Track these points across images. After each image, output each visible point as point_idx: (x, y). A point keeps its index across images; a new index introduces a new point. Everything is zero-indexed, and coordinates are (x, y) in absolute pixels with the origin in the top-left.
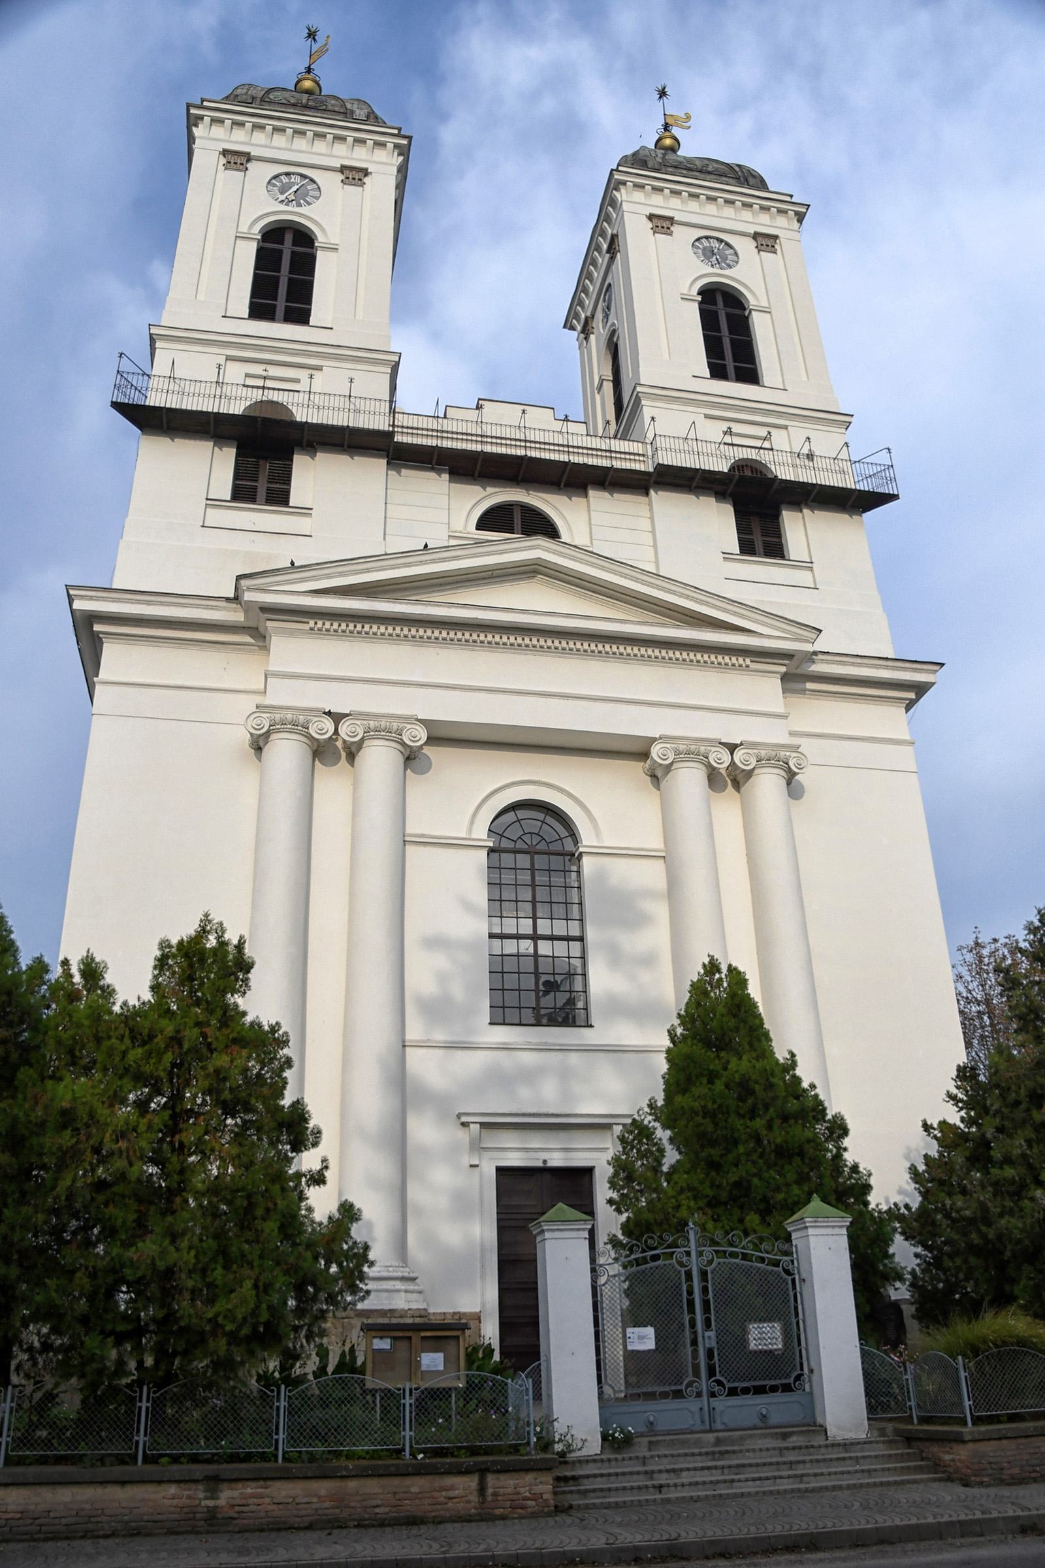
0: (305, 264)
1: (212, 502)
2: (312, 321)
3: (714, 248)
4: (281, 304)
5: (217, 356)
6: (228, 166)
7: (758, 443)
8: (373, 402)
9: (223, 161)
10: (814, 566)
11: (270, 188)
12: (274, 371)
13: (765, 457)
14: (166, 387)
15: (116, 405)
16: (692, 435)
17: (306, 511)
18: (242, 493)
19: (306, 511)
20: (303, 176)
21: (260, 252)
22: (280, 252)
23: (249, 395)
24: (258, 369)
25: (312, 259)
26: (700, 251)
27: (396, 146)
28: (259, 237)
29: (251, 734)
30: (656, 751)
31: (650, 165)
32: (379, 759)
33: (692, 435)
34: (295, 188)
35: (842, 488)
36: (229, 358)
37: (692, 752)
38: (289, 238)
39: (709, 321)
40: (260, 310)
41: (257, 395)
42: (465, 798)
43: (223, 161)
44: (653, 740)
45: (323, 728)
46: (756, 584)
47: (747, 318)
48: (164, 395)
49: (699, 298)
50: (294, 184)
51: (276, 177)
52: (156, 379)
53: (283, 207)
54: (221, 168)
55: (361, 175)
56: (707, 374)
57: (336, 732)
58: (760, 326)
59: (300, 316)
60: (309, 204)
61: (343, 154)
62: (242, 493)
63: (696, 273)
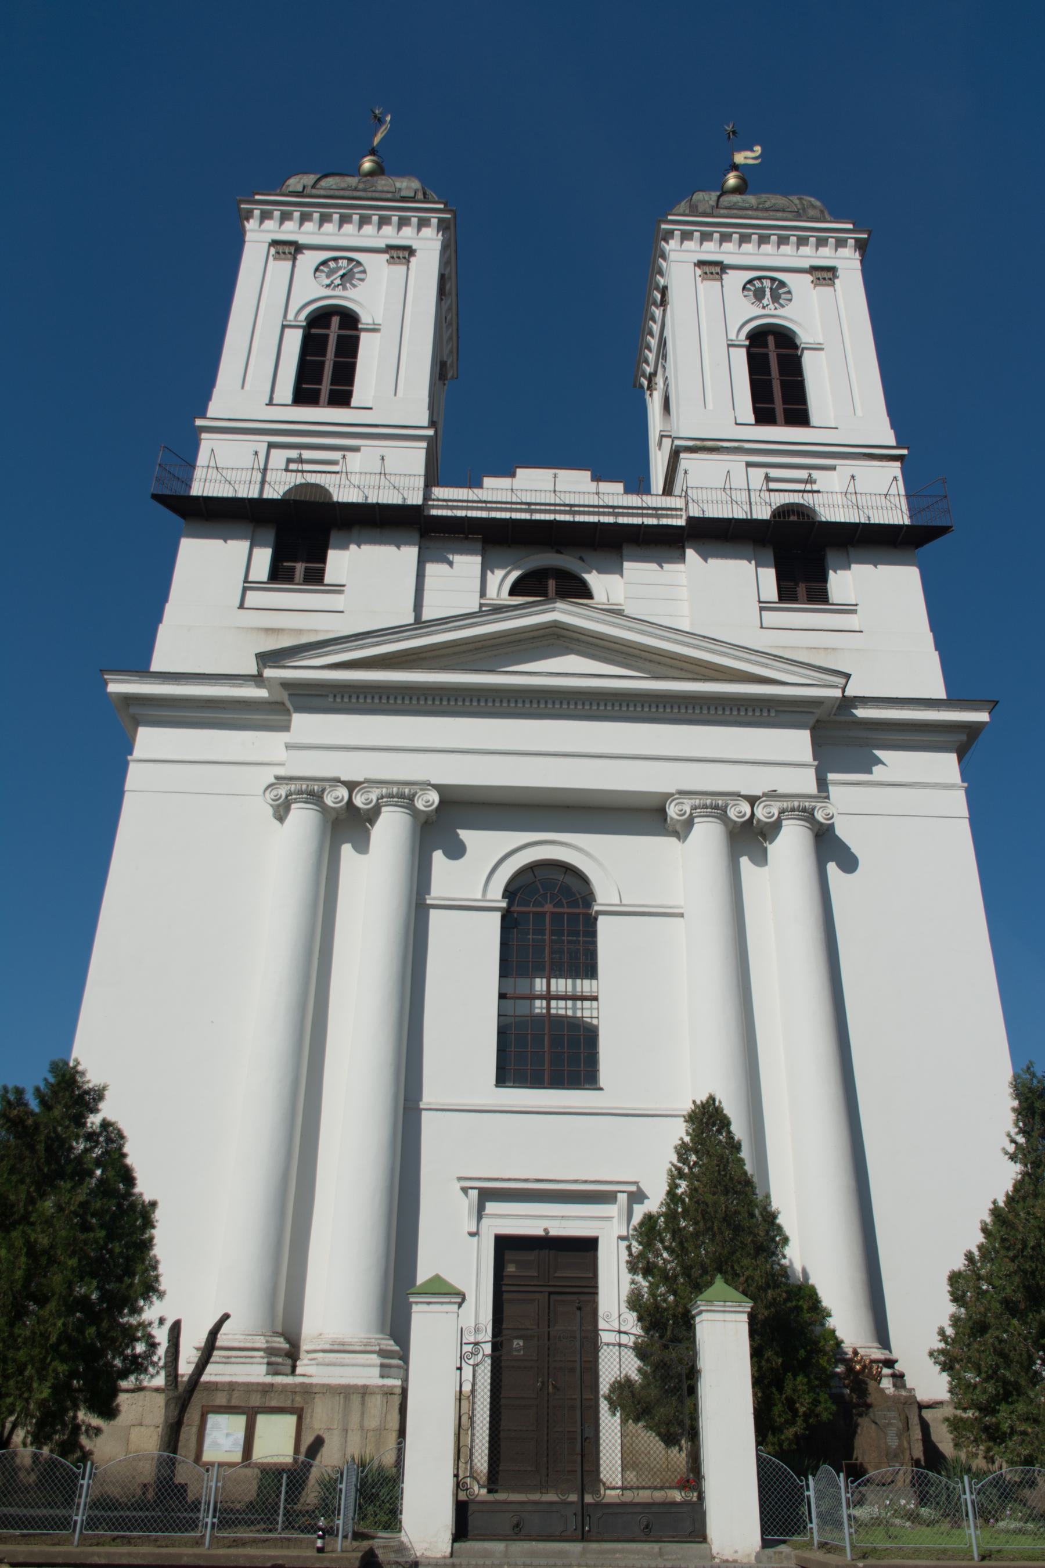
0: (349, 348)
1: (764, 607)
2: (353, 404)
3: (767, 286)
4: (325, 387)
5: (260, 443)
6: (705, 276)
7: (801, 487)
8: (709, 491)
9: (699, 272)
10: (757, 605)
11: (746, 293)
12: (307, 454)
13: (807, 500)
14: (377, 484)
15: (156, 497)
16: (212, 464)
17: (849, 609)
18: (279, 574)
19: (849, 609)
20: (350, 260)
21: (751, 357)
22: (327, 336)
23: (288, 480)
24: (294, 454)
25: (357, 339)
26: (751, 293)
27: (857, 240)
28: (304, 324)
29: (271, 805)
30: (672, 811)
31: (700, 210)
32: (707, 834)
33: (851, 490)
34: (341, 272)
35: (699, 518)
36: (749, 465)
37: (714, 806)
38: (335, 321)
39: (757, 365)
40: (303, 396)
41: (300, 479)
42: (484, 864)
43: (273, 251)
44: (668, 796)
45: (740, 811)
46: (799, 631)
47: (800, 357)
48: (376, 491)
49: (747, 343)
50: (340, 268)
51: (750, 282)
52: (274, 473)
53: (328, 292)
54: (699, 279)
55: (718, 269)
56: (751, 419)
57: (753, 814)
58: (812, 366)
59: (342, 398)
60: (783, 306)
61: (390, 235)
62: (279, 574)
63: (746, 313)
